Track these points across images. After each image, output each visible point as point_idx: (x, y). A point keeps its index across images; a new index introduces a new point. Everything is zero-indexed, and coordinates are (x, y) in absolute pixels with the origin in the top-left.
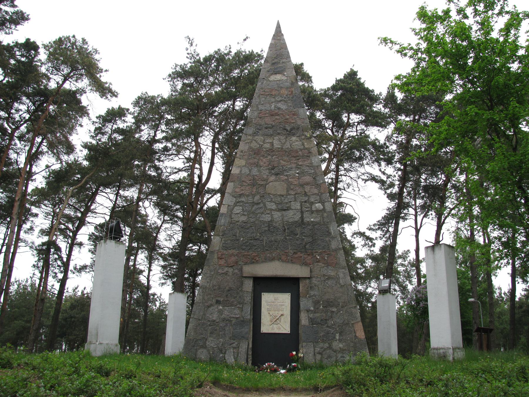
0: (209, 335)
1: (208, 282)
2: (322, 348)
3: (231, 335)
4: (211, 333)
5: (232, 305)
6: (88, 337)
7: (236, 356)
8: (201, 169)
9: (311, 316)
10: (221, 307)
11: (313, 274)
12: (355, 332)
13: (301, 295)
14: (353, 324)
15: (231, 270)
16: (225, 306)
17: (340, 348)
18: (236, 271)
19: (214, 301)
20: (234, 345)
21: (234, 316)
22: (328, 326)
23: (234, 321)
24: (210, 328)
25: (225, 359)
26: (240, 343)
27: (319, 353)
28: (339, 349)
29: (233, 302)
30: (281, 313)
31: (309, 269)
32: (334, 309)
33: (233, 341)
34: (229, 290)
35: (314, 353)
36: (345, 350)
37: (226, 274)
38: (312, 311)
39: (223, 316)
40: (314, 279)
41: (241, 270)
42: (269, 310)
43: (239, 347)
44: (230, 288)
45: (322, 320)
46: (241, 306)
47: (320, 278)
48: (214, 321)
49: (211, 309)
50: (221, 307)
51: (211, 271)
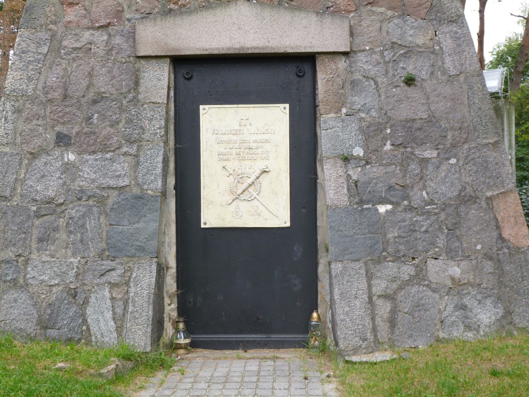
0: (34, 245)
1: (30, 79)
2: (393, 280)
3: (103, 245)
4: (40, 240)
5: (105, 149)
6: (319, 238)
7: (119, 311)
8: (207, 354)
9: (355, 173)
10: (72, 157)
11: (357, 41)
12: (498, 227)
13: (321, 108)
14: (490, 199)
15: (101, 37)
16: (85, 151)
17: (453, 279)
18: (118, 40)
19: (50, 136)
20: (114, 277)
21: (112, 183)
22: (410, 208)
23: (113, 197)
24: (37, 222)
25: (85, 321)
26: (130, 270)
27: (386, 297)
28: (449, 283)
29: (108, 137)
30: (260, 165)
31: (346, 26)
32: (430, 153)
33: (108, 264)
34: (95, 102)
35: (370, 298)
36: (469, 283)
37: (87, 49)
38: (358, 158)
39: (79, 183)
40: (361, 57)
41: (132, 36)
42: (223, 157)
43: (127, 284)
44: (99, 93)
45: (390, 188)
46: (133, 150)
47: (382, 53)
48: (50, 201)
49: (39, 163)
50: (72, 157)
51: (39, 44)
